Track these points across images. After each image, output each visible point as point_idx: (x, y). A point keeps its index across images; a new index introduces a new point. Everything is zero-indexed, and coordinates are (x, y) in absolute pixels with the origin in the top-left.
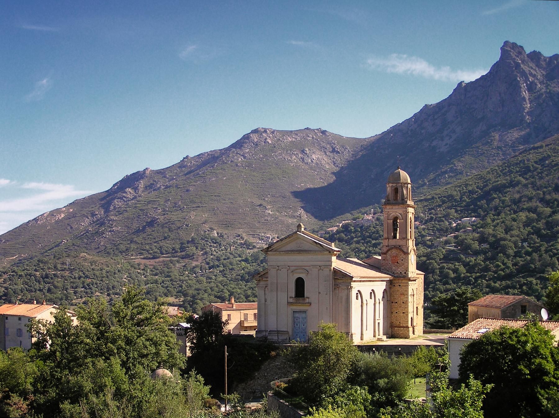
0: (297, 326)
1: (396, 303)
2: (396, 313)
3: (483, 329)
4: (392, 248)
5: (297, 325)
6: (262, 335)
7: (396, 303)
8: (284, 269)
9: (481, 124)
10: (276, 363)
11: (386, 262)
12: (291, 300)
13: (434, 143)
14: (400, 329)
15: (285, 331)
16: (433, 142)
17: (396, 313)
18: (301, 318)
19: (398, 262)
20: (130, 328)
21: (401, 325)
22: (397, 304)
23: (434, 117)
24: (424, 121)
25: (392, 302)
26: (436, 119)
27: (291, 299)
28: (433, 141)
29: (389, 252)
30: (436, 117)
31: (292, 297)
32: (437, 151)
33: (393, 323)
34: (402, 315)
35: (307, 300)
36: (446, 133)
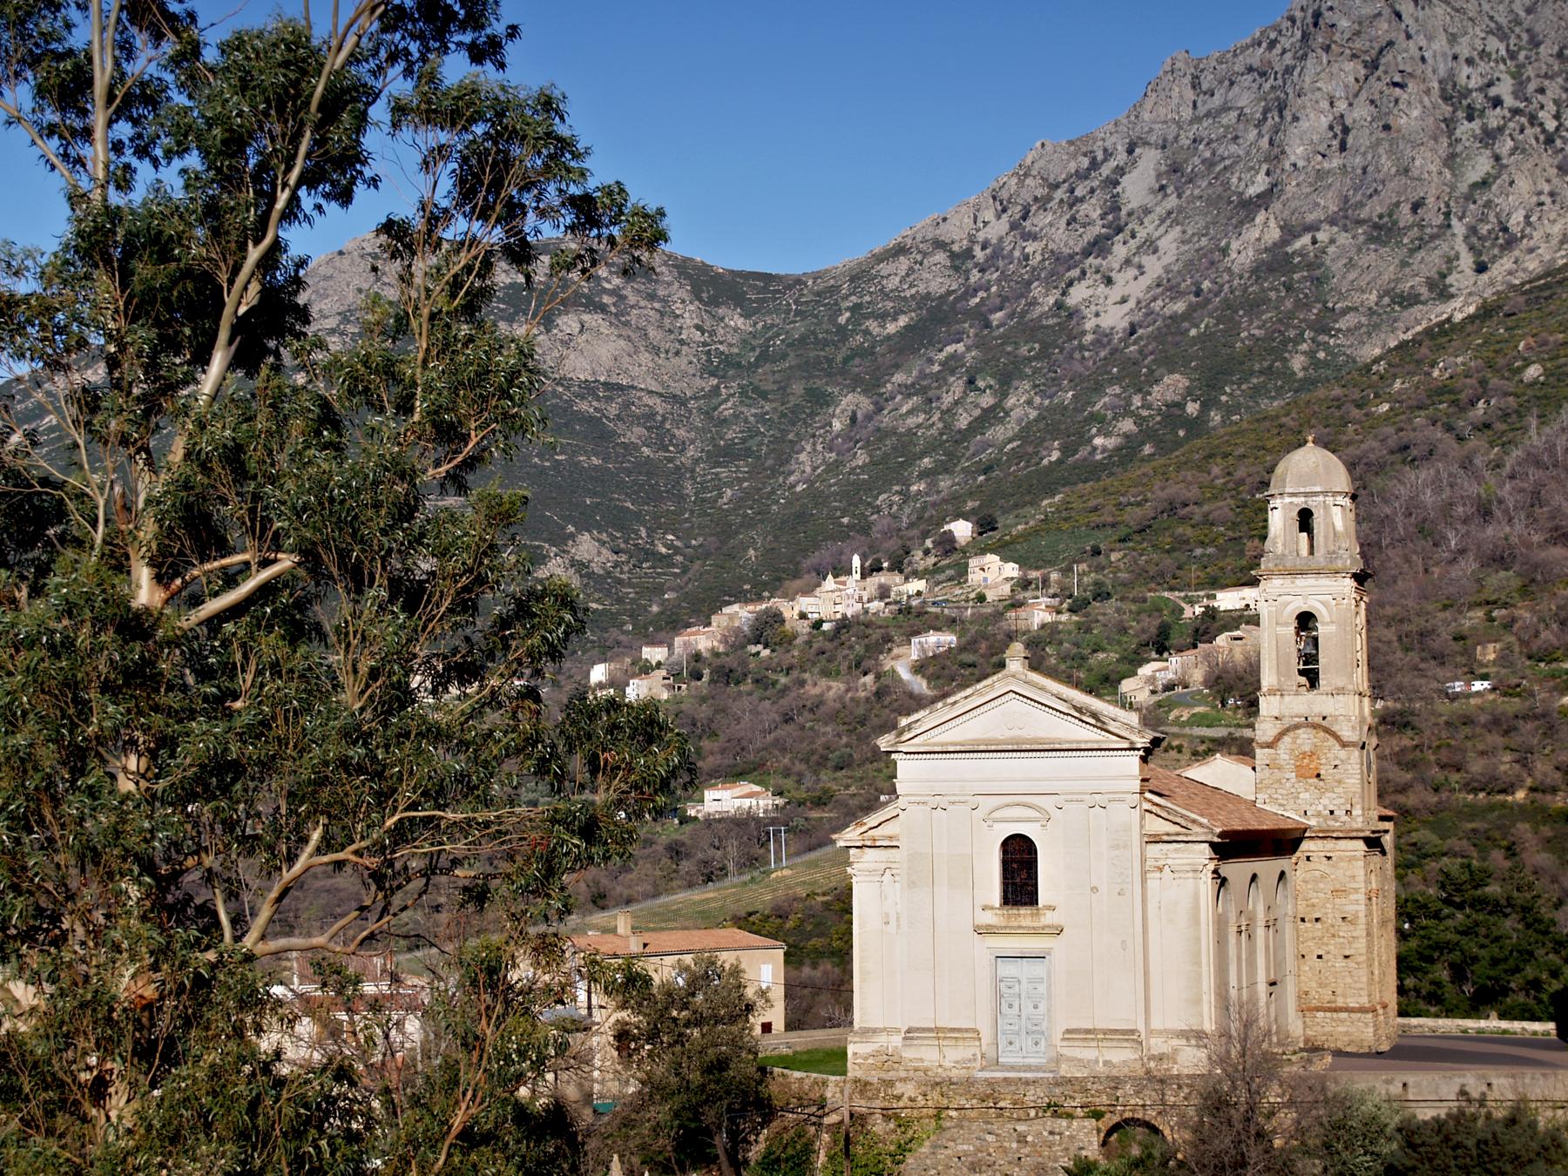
0: (1009, 1011)
1: (1317, 920)
2: (1320, 957)
3: (1300, 1023)
4: (1297, 727)
5: (1011, 1006)
6: (876, 1047)
7: (1317, 920)
8: (1074, 805)
9: (1260, 218)
10: (960, 1147)
11: (1277, 774)
12: (989, 918)
13: (1078, 294)
14: (1335, 1015)
15: (967, 1030)
16: (1072, 290)
17: (1320, 957)
18: (1024, 982)
19: (1318, 775)
20: (366, 1027)
21: (1340, 1002)
22: (1318, 925)
23: (1072, 191)
24: (1034, 208)
25: (1303, 920)
26: (1082, 200)
27: (989, 913)
28: (1070, 284)
29: (1287, 739)
30: (1079, 192)
31: (992, 908)
32: (1089, 325)
33: (1306, 993)
34: (1340, 964)
35: (1048, 918)
36: (1120, 250)
